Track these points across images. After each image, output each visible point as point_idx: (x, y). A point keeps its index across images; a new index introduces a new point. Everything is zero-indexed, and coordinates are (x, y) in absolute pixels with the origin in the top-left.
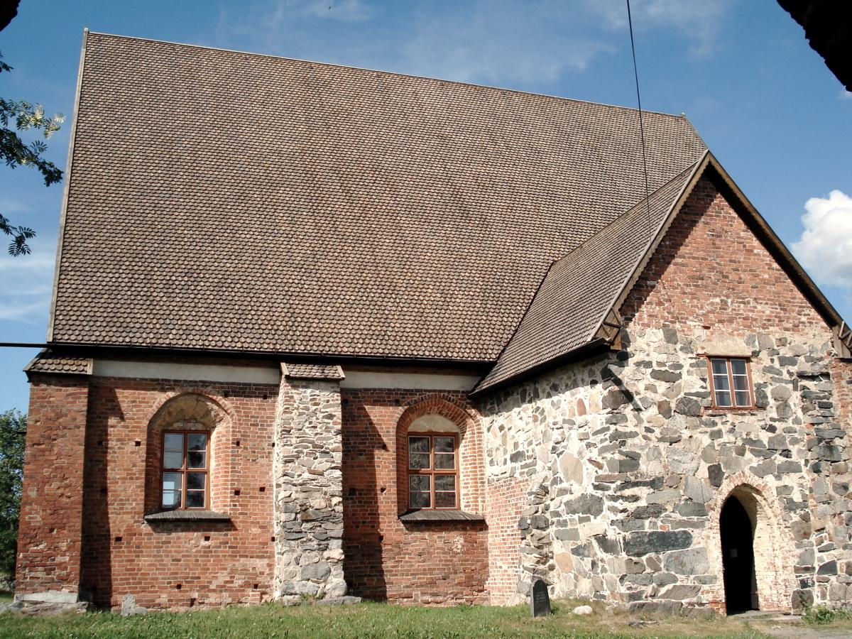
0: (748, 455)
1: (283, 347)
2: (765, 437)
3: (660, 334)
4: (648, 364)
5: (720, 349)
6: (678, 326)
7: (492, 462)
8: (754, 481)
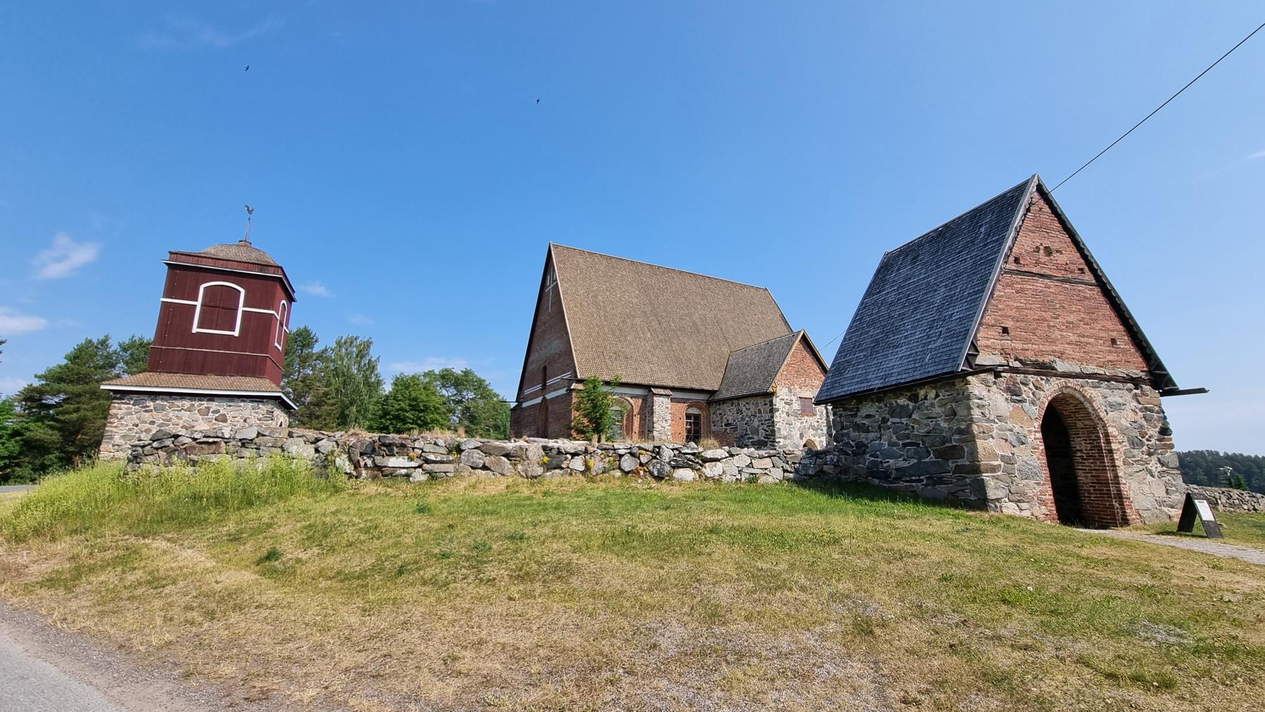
0: (811, 430)
1: (651, 383)
2: (816, 424)
3: (787, 389)
4: (784, 400)
5: (803, 395)
6: (792, 387)
7: (714, 426)
8: (812, 438)
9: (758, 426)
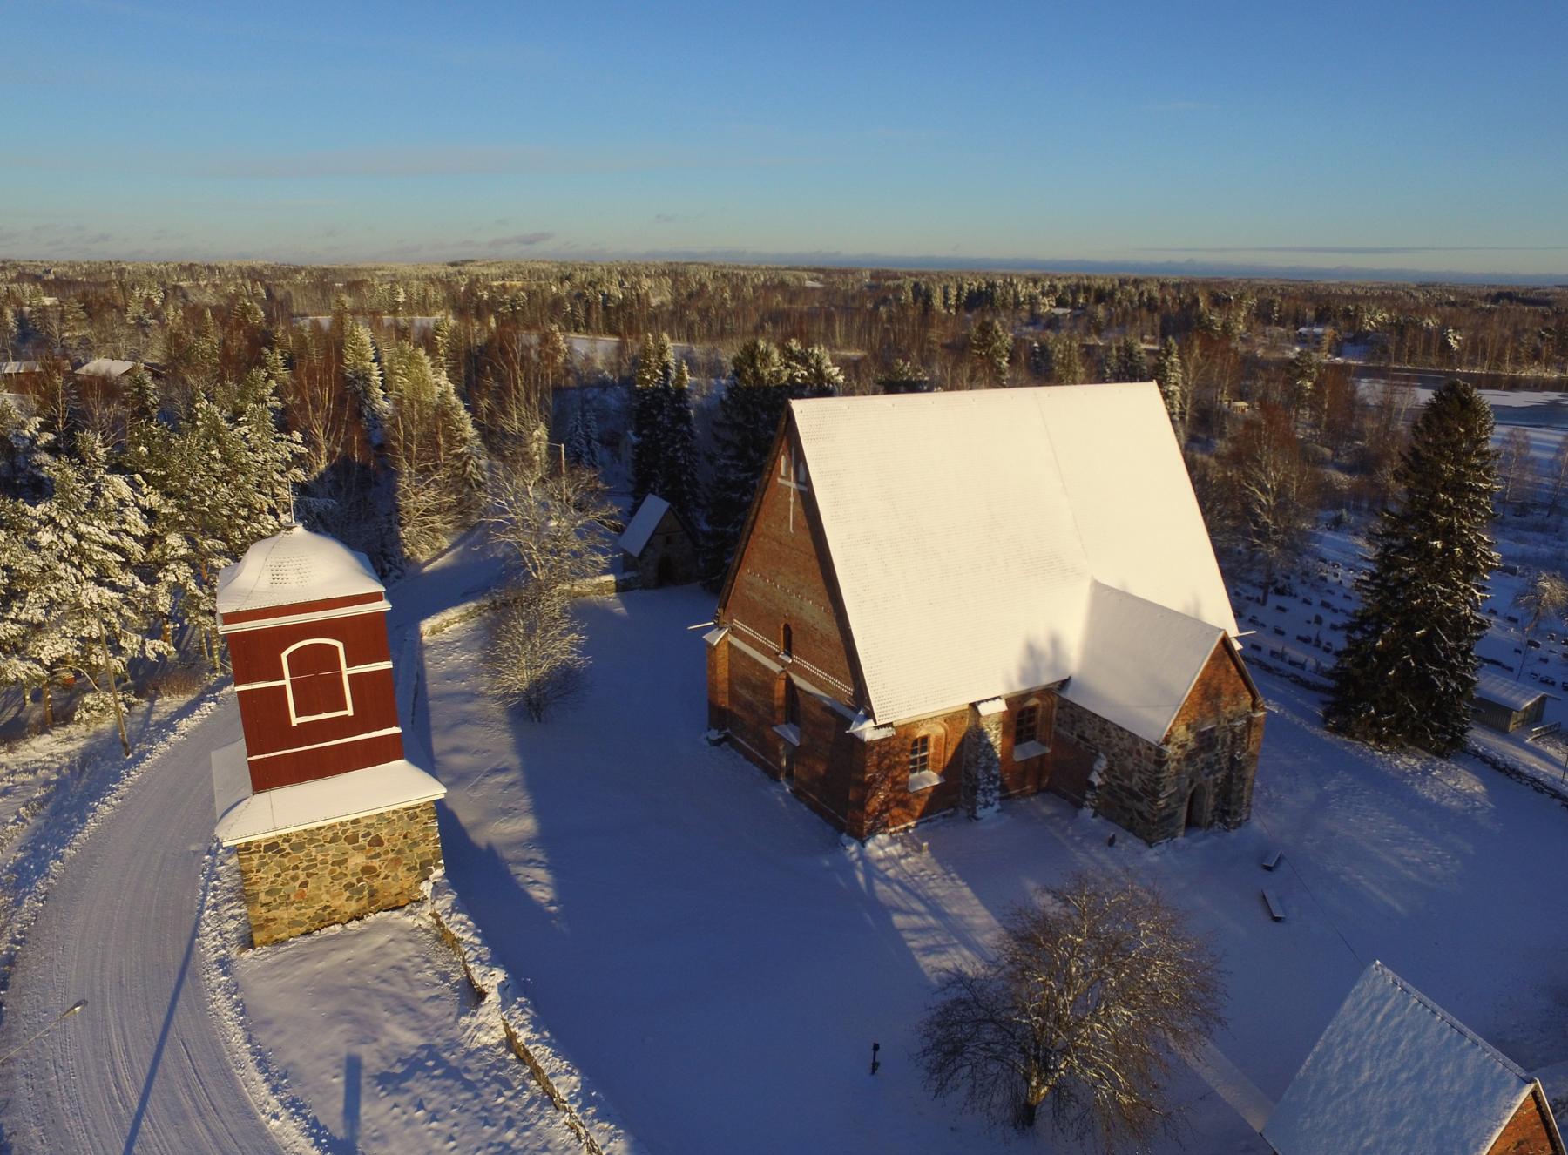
9: (1133, 770)
